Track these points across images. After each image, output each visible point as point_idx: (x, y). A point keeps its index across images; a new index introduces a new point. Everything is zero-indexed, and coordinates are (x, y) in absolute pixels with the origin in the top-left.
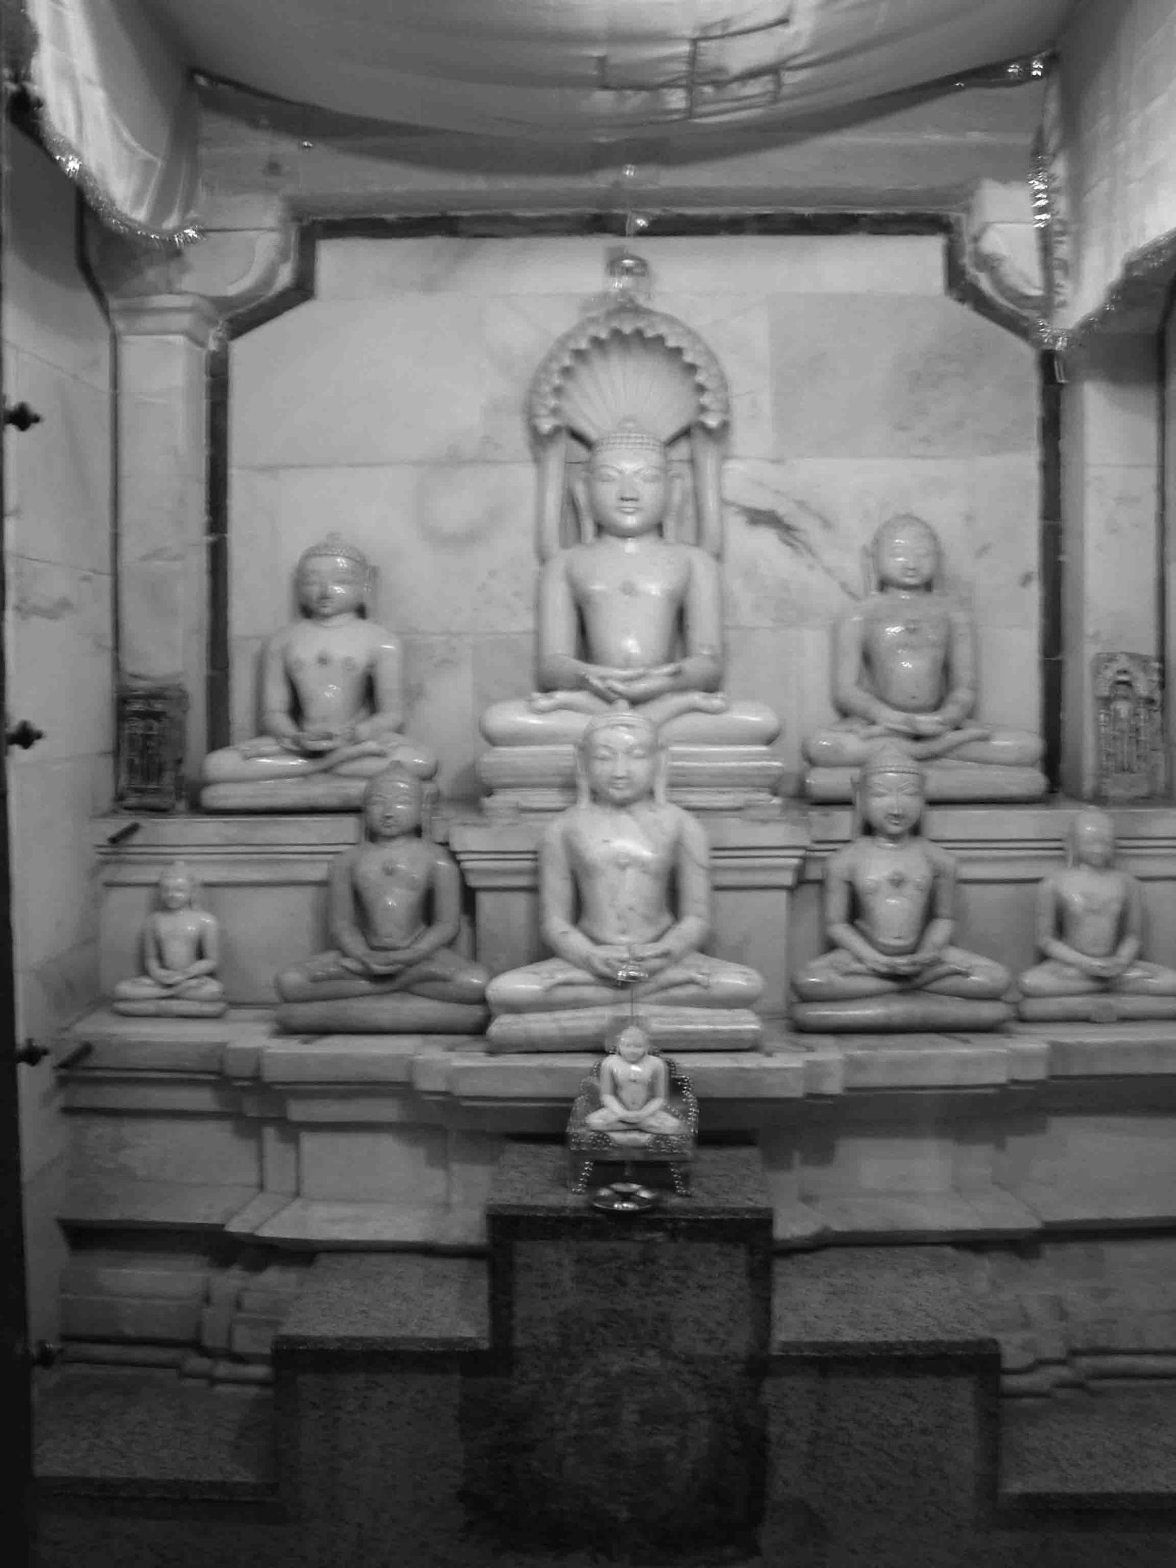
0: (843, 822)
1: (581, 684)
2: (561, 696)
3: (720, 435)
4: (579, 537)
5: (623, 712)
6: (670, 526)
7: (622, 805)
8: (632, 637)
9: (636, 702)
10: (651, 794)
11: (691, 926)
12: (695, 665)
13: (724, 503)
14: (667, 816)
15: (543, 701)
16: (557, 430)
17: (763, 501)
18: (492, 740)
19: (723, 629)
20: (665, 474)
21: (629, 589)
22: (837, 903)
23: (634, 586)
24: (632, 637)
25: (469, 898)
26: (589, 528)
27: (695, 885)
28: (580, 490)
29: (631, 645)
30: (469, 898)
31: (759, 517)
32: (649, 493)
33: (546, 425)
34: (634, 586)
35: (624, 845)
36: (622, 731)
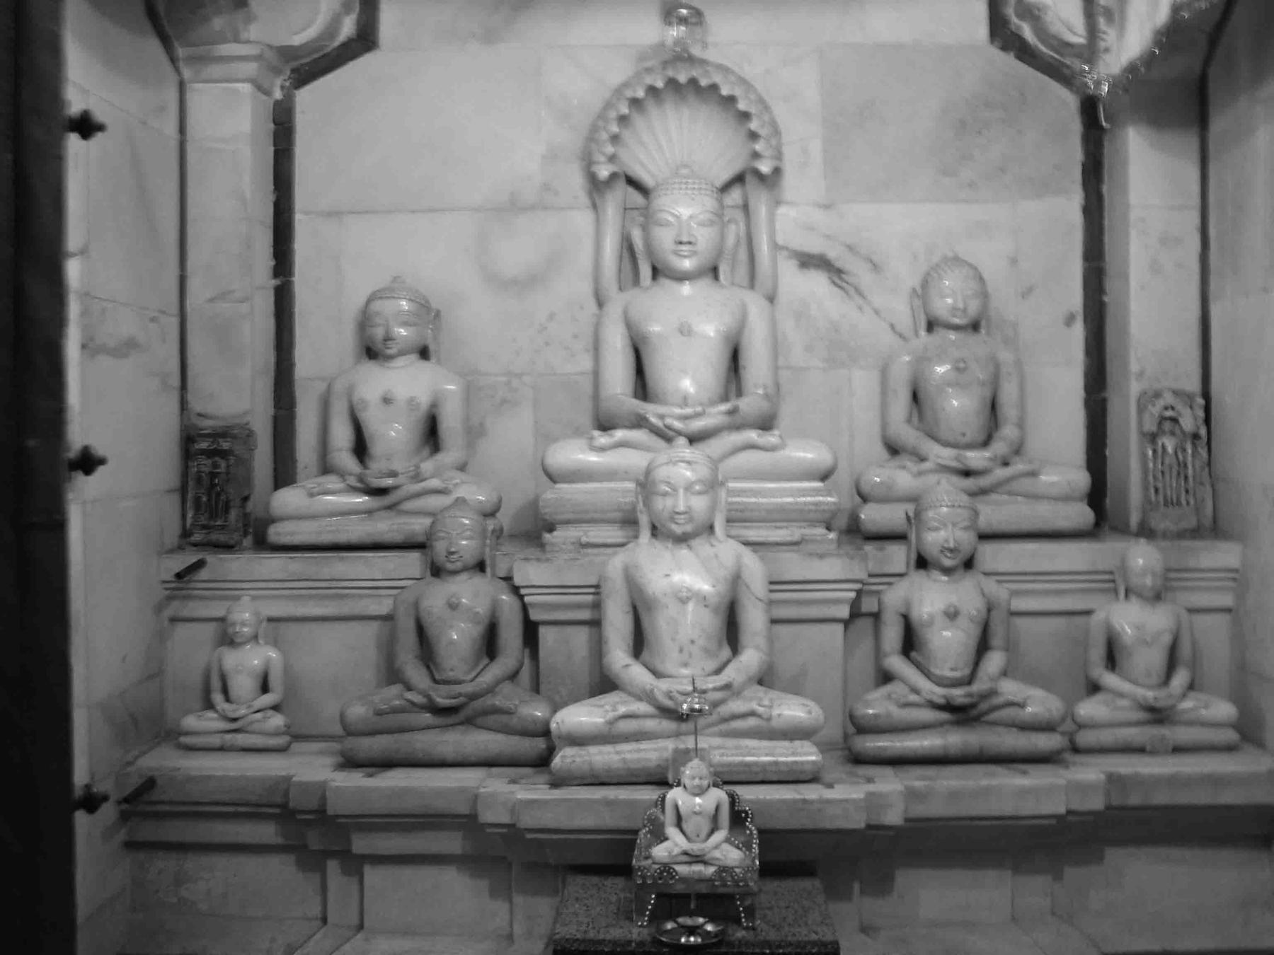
0: (897, 556)
1: (640, 422)
3: (771, 181)
4: (636, 281)
5: (682, 449)
6: (723, 269)
7: (682, 540)
9: (693, 439)
10: (711, 528)
11: (751, 658)
12: (750, 404)
13: (776, 247)
15: (602, 439)
16: (614, 176)
17: (814, 246)
20: (719, 218)
21: (685, 331)
22: (892, 635)
24: (688, 377)
26: (645, 271)
27: (754, 619)
29: (687, 385)
30: (530, 632)
31: (808, 261)
32: (704, 238)
33: (604, 172)
34: (689, 328)
35: (683, 579)
36: (682, 469)
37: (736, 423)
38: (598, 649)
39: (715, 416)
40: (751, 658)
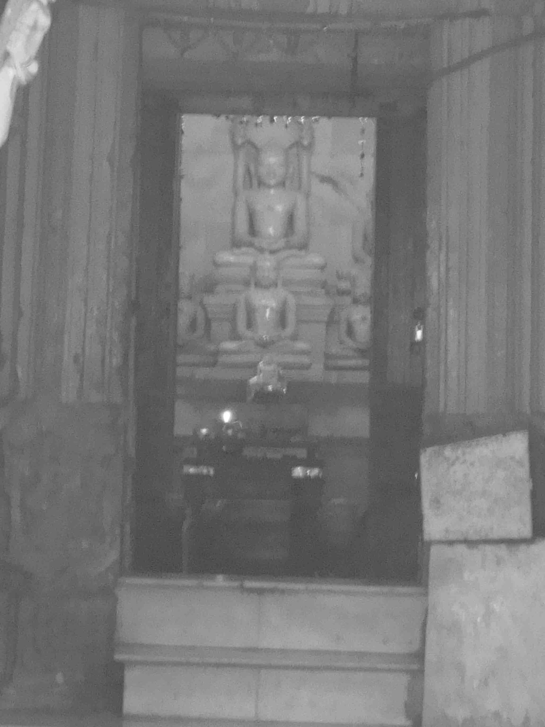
0: (348, 300)
1: (251, 245)
2: (244, 249)
3: (310, 147)
4: (251, 186)
5: (267, 256)
6: (288, 183)
7: (267, 287)
8: (271, 228)
9: (272, 252)
10: (276, 285)
11: (289, 330)
12: (296, 239)
13: (310, 173)
14: (282, 292)
15: (237, 251)
16: (243, 144)
17: (326, 172)
18: (216, 265)
19: (308, 224)
20: (287, 164)
21: (270, 208)
22: (343, 327)
23: (273, 206)
24: (271, 228)
25: (208, 322)
26: (255, 182)
27: (291, 318)
28: (252, 169)
29: (271, 231)
30: (208, 322)
31: (325, 179)
32: (280, 171)
33: (240, 141)
34: (273, 206)
35: (267, 303)
36: (267, 263)
37: (288, 246)
38: (234, 329)
39: (281, 243)
40: (289, 330)
